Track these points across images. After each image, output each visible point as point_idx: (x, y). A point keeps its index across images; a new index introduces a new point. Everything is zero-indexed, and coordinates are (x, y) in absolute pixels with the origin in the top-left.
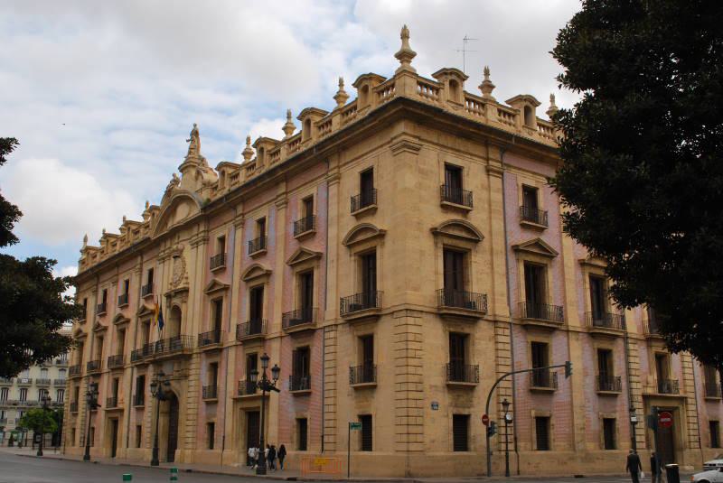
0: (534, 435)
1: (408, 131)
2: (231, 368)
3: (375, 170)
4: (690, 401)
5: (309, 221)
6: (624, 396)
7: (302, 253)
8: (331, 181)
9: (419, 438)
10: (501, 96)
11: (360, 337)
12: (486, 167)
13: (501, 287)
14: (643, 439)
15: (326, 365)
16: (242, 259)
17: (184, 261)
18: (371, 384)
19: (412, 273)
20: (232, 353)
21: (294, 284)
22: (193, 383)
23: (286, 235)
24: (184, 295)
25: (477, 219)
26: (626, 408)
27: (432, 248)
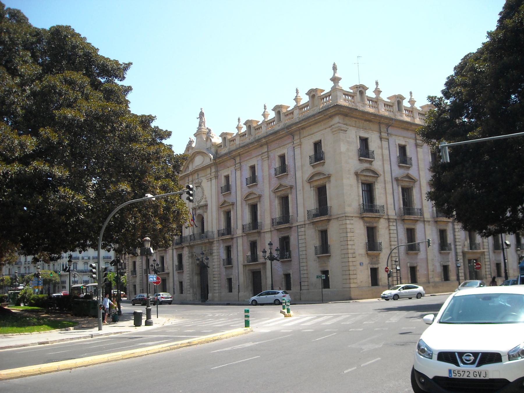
0: (410, 276)
1: (341, 121)
2: (240, 248)
4: (486, 253)
5: (283, 168)
6: (452, 253)
7: (281, 185)
9: (355, 281)
10: (384, 96)
11: (319, 231)
13: (390, 200)
14: (463, 275)
15: (300, 246)
16: (242, 188)
17: (202, 189)
18: (461, 275)
19: (347, 195)
20: (240, 241)
21: (276, 203)
22: (216, 257)
23: (270, 175)
24: (205, 208)
25: (377, 165)
26: (454, 260)
27: (356, 183)
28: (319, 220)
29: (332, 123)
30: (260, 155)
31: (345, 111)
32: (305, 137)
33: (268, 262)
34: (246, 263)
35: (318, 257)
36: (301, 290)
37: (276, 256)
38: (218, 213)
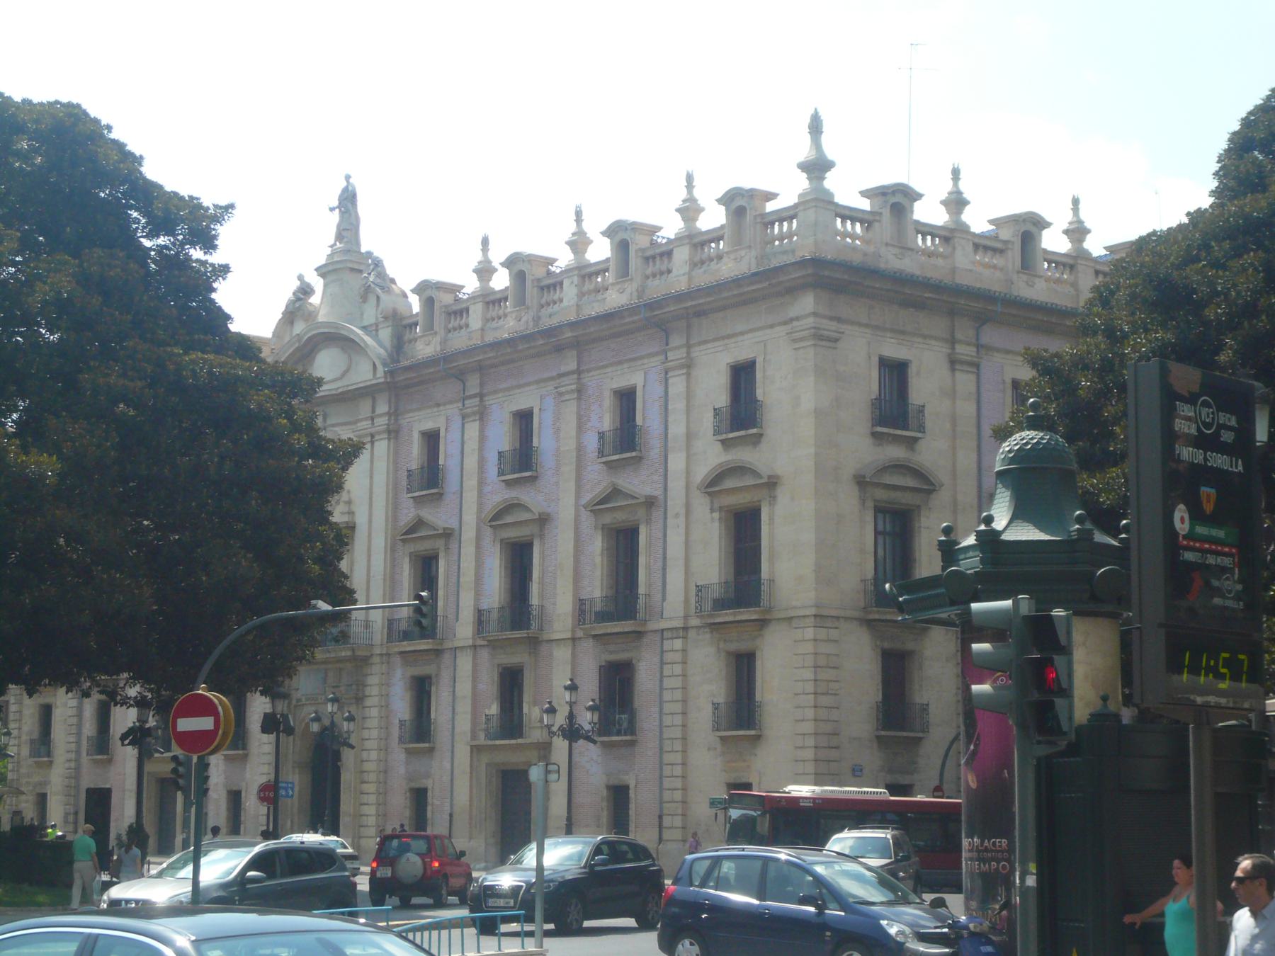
2: (464, 688)
3: (758, 366)
7: (615, 493)
8: (673, 369)
12: (949, 355)
16: (481, 483)
20: (465, 664)
21: (596, 546)
23: (580, 449)
25: (932, 452)
28: (731, 618)
29: (793, 311)
30: (552, 379)
31: (838, 275)
32: (706, 342)
33: (560, 745)
34: (482, 740)
35: (721, 738)
36: (660, 840)
37: (587, 727)
38: (393, 560)
